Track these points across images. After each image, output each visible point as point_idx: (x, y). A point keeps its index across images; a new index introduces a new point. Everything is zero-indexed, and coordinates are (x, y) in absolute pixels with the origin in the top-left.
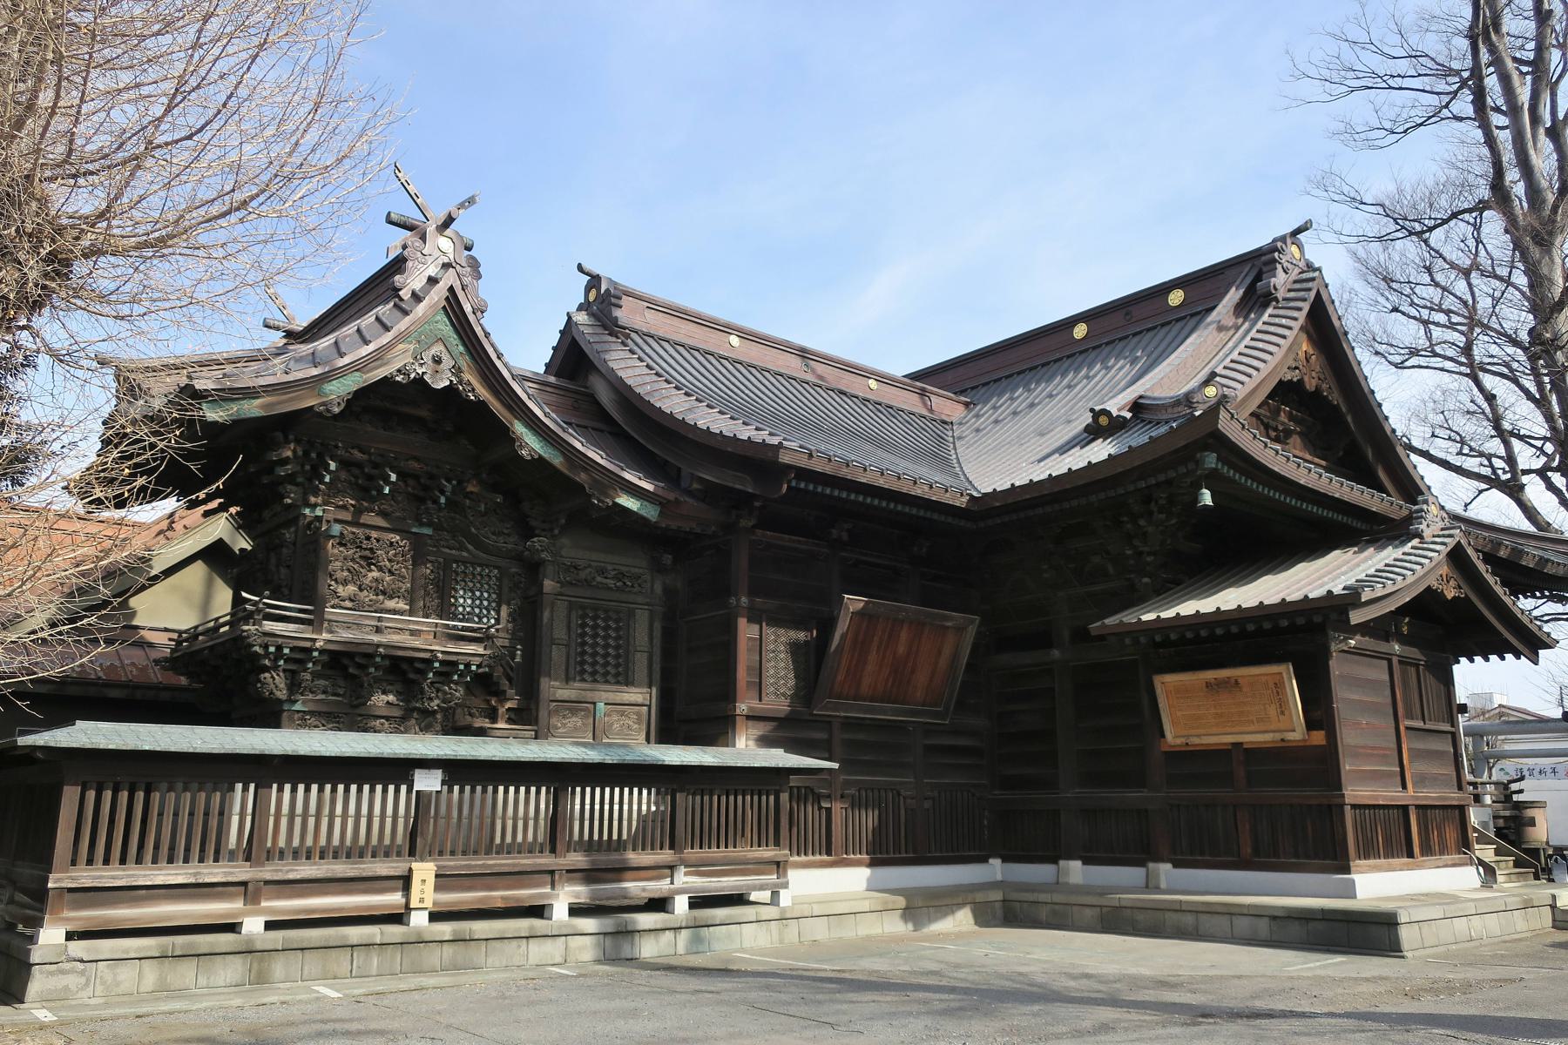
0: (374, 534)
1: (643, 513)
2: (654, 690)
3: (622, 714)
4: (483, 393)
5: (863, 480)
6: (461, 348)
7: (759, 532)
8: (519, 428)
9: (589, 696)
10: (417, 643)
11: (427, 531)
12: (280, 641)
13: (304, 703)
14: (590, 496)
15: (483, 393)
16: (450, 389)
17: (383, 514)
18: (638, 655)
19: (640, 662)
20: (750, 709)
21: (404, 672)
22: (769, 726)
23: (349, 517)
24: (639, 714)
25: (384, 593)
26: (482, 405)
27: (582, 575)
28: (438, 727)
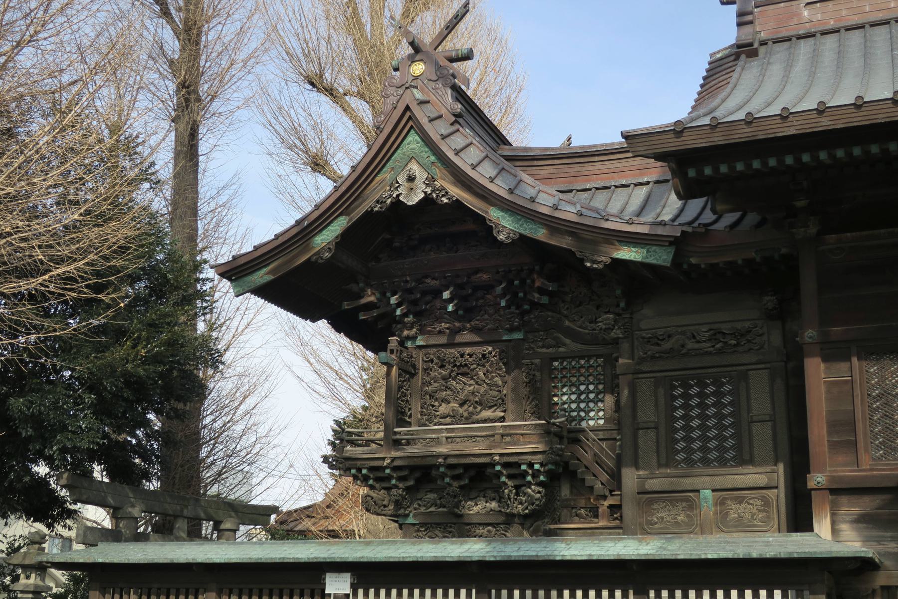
0: (468, 350)
1: (651, 260)
2: (781, 467)
3: (740, 501)
4: (456, 192)
5: (792, 131)
6: (433, 158)
7: (832, 238)
8: (494, 215)
9: (687, 483)
10: (477, 450)
11: (518, 336)
12: (359, 463)
13: (415, 516)
14: (582, 261)
15: (456, 192)
16: (427, 200)
17: (475, 330)
18: (756, 428)
19: (762, 434)
20: (832, 479)
21: (477, 477)
22: (867, 504)
23: (443, 340)
24: (766, 503)
25: (479, 403)
26: (457, 204)
27: (666, 346)
28: (184, 535)
